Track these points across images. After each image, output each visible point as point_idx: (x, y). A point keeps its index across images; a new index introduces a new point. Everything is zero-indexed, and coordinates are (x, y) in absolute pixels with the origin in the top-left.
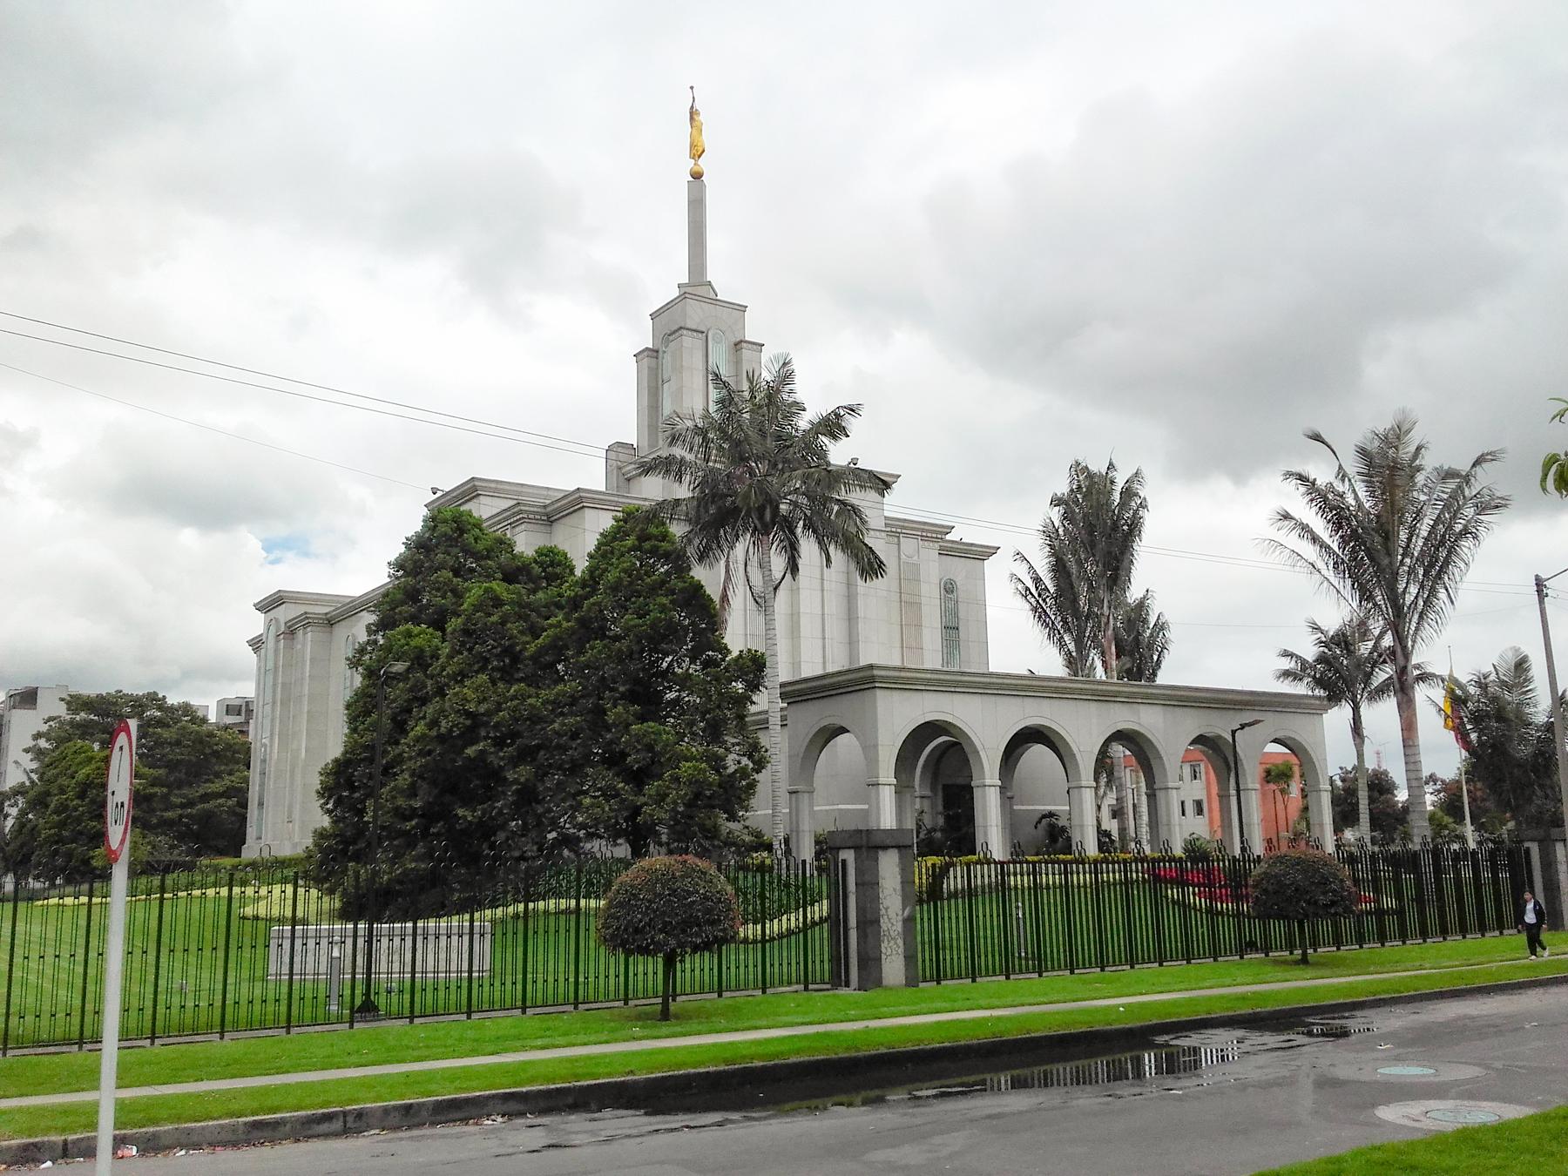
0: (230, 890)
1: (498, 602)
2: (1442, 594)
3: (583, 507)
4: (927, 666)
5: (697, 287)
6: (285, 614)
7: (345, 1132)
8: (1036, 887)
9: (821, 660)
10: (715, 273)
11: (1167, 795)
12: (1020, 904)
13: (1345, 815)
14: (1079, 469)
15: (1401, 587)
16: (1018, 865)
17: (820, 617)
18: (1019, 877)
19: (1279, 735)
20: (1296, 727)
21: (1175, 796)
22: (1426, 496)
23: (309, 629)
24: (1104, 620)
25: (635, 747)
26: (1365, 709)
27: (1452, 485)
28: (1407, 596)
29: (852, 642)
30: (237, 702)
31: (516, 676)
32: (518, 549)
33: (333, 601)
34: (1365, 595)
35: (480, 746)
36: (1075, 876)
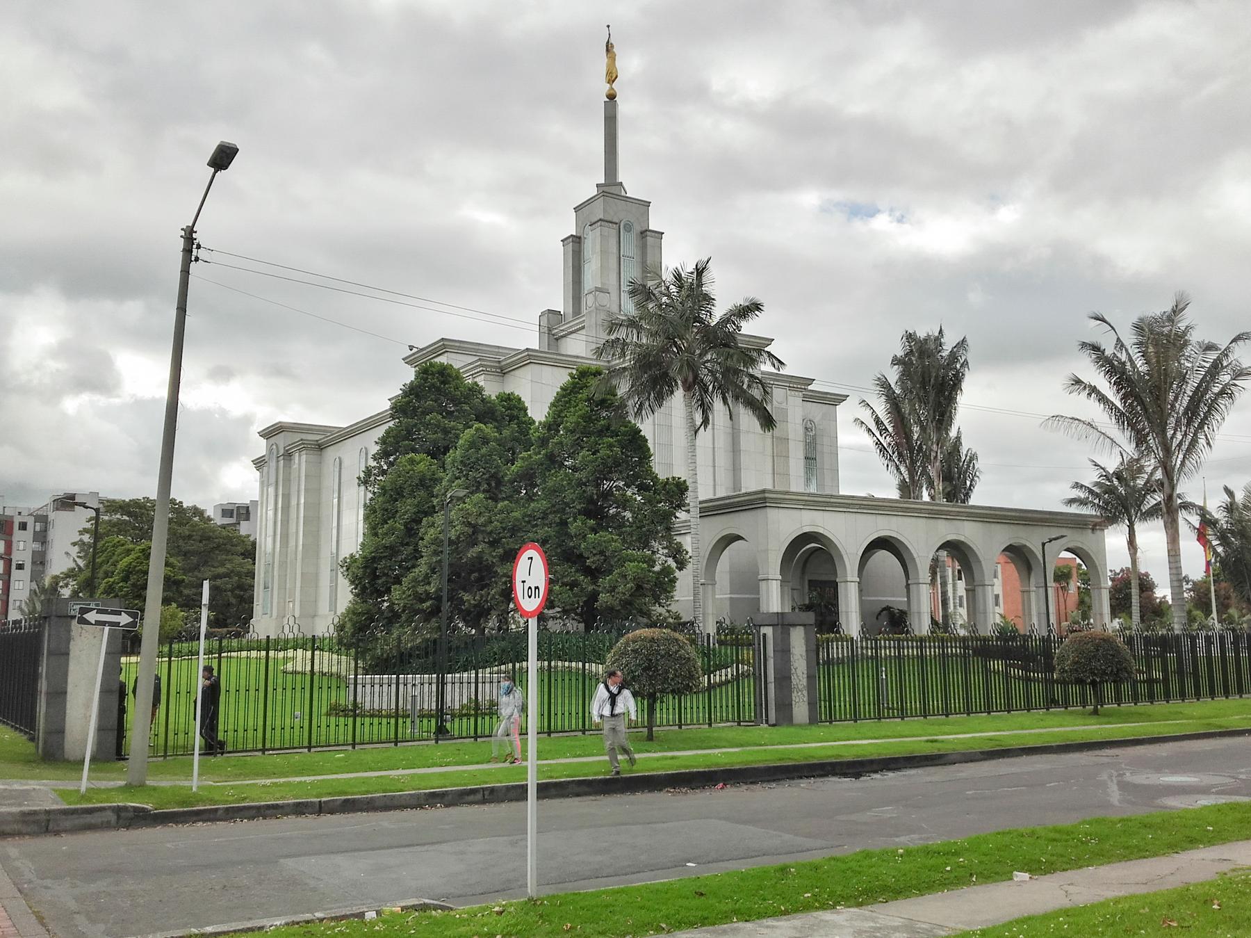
0: (267, 653)
1: (485, 441)
2: (1202, 441)
3: (531, 362)
4: (793, 489)
5: (610, 188)
6: (282, 441)
7: (484, 801)
8: (899, 657)
9: (712, 483)
10: (622, 177)
11: (768, 585)
12: (884, 669)
13: (1120, 604)
14: (910, 337)
15: (1170, 433)
16: (892, 642)
17: (711, 450)
18: (892, 649)
19: (1070, 545)
20: (1084, 540)
21: (990, 591)
22: (1194, 363)
23: (304, 452)
24: (933, 454)
25: (592, 552)
26: (1138, 526)
27: (1213, 356)
28: (1174, 439)
29: (736, 469)
30: (230, 507)
31: (500, 496)
32: (486, 393)
33: (324, 431)
34: (1140, 440)
35: (478, 549)
36: (928, 650)
